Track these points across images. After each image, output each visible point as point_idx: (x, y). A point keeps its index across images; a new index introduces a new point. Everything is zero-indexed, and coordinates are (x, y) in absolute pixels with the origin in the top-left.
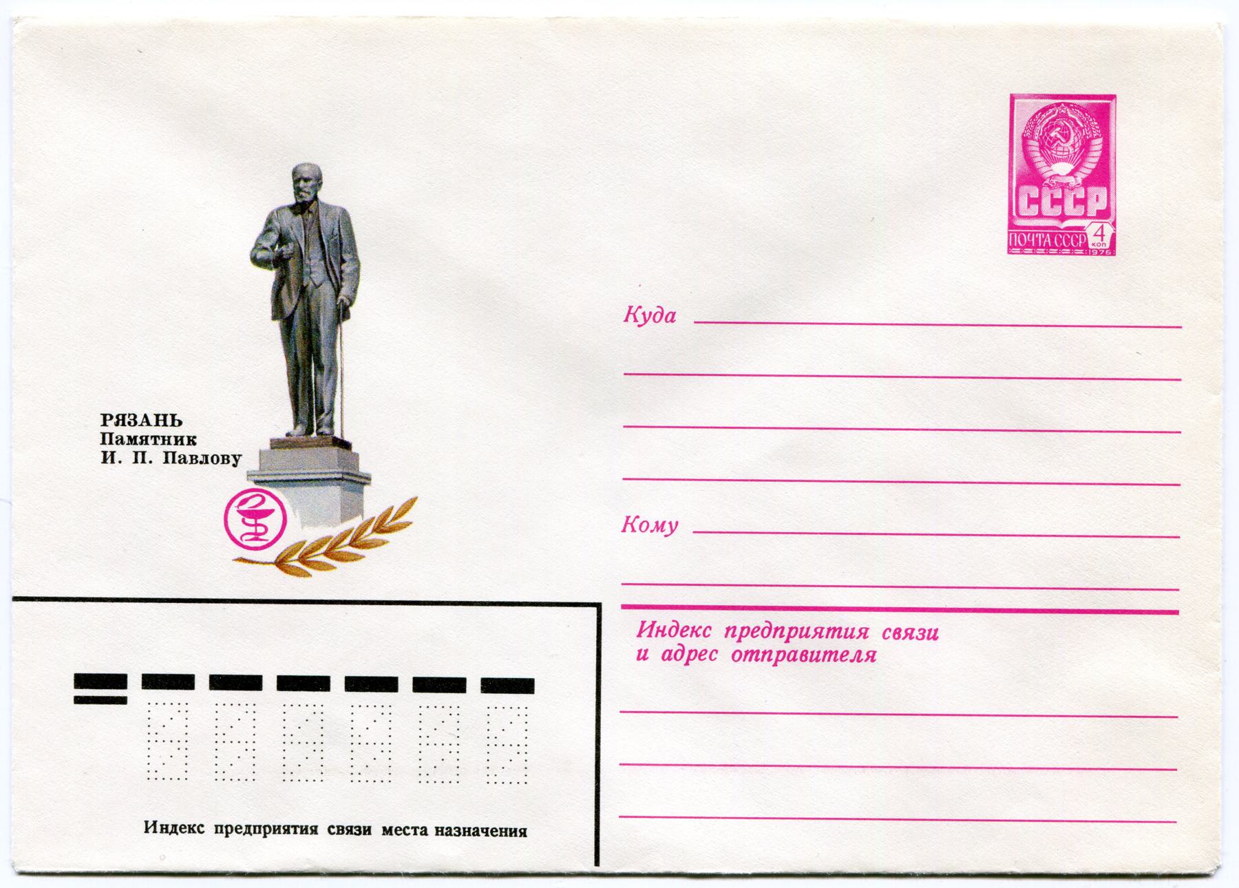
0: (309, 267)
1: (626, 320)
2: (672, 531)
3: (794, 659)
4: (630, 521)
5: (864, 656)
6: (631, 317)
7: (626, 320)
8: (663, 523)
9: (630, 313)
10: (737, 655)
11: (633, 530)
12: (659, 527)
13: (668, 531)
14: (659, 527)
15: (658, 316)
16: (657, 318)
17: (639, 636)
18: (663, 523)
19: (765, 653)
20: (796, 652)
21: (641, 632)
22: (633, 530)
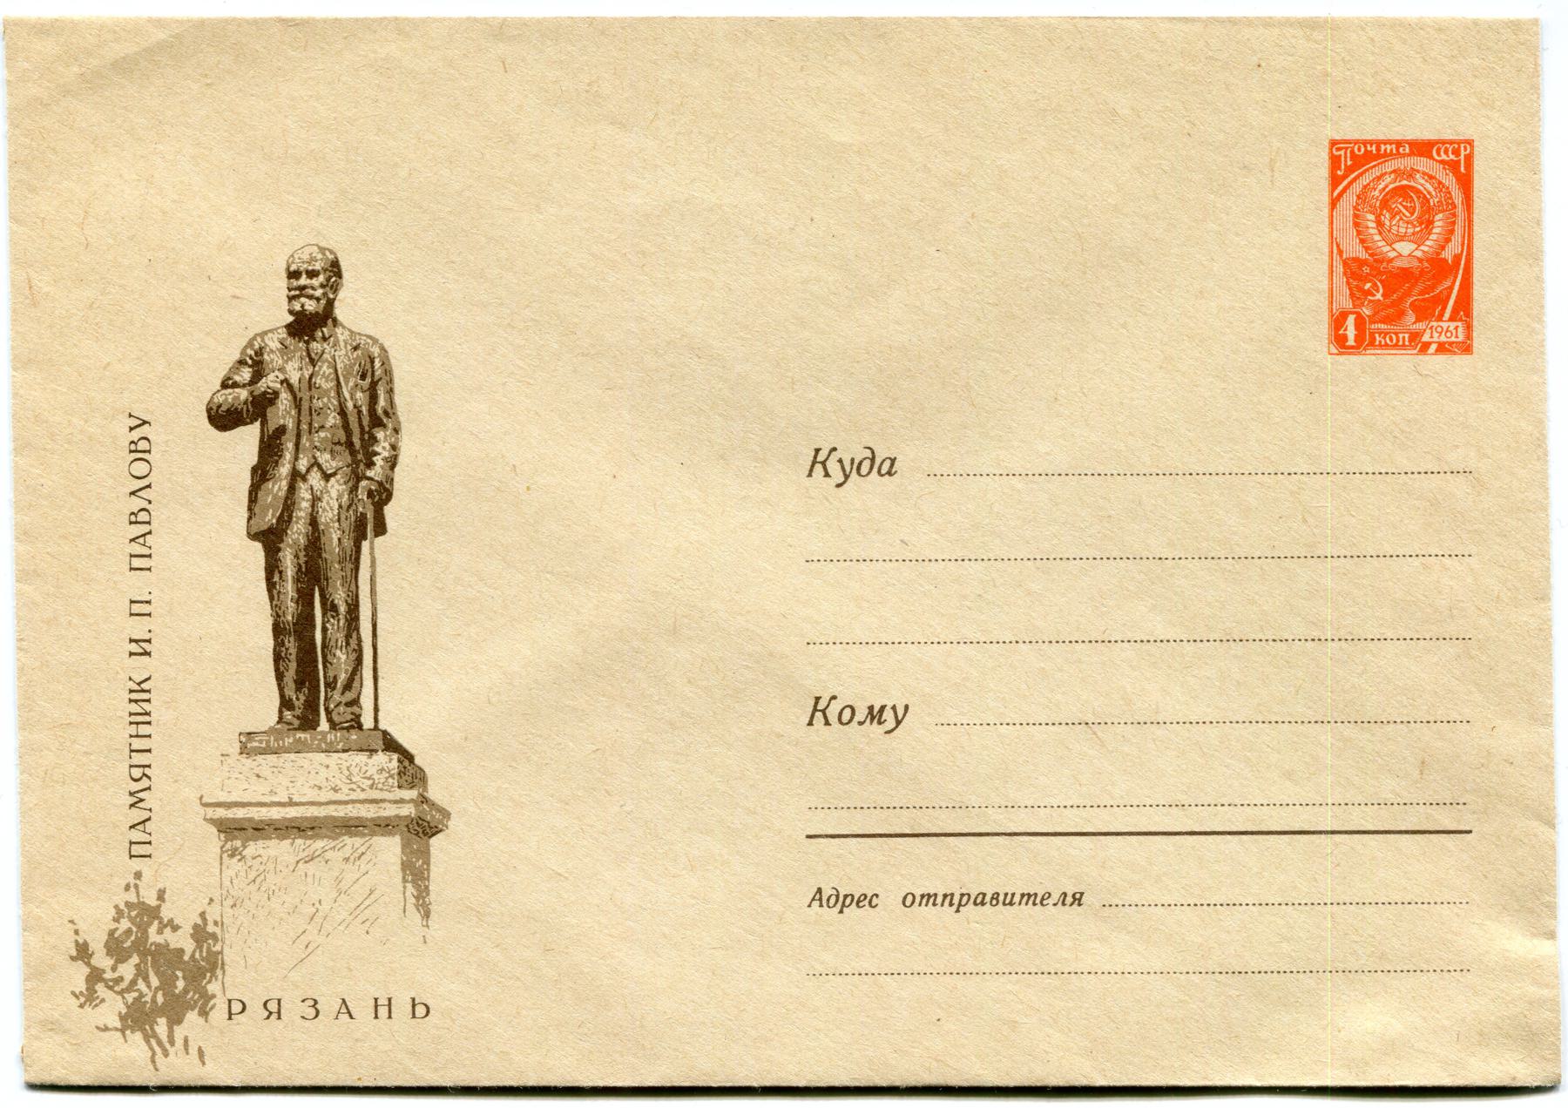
0: (313, 433)
1: (810, 724)
2: (898, 723)
3: (983, 903)
4: (821, 458)
5: (1069, 899)
6: (819, 467)
7: (810, 724)
8: (883, 708)
9: (818, 462)
10: (910, 898)
11: (827, 723)
12: (875, 715)
13: (891, 724)
14: (875, 715)
15: (866, 464)
16: (864, 470)
17: (131, 641)
18: (883, 708)
19: (945, 896)
20: (984, 895)
21: (136, 641)
22: (827, 723)
